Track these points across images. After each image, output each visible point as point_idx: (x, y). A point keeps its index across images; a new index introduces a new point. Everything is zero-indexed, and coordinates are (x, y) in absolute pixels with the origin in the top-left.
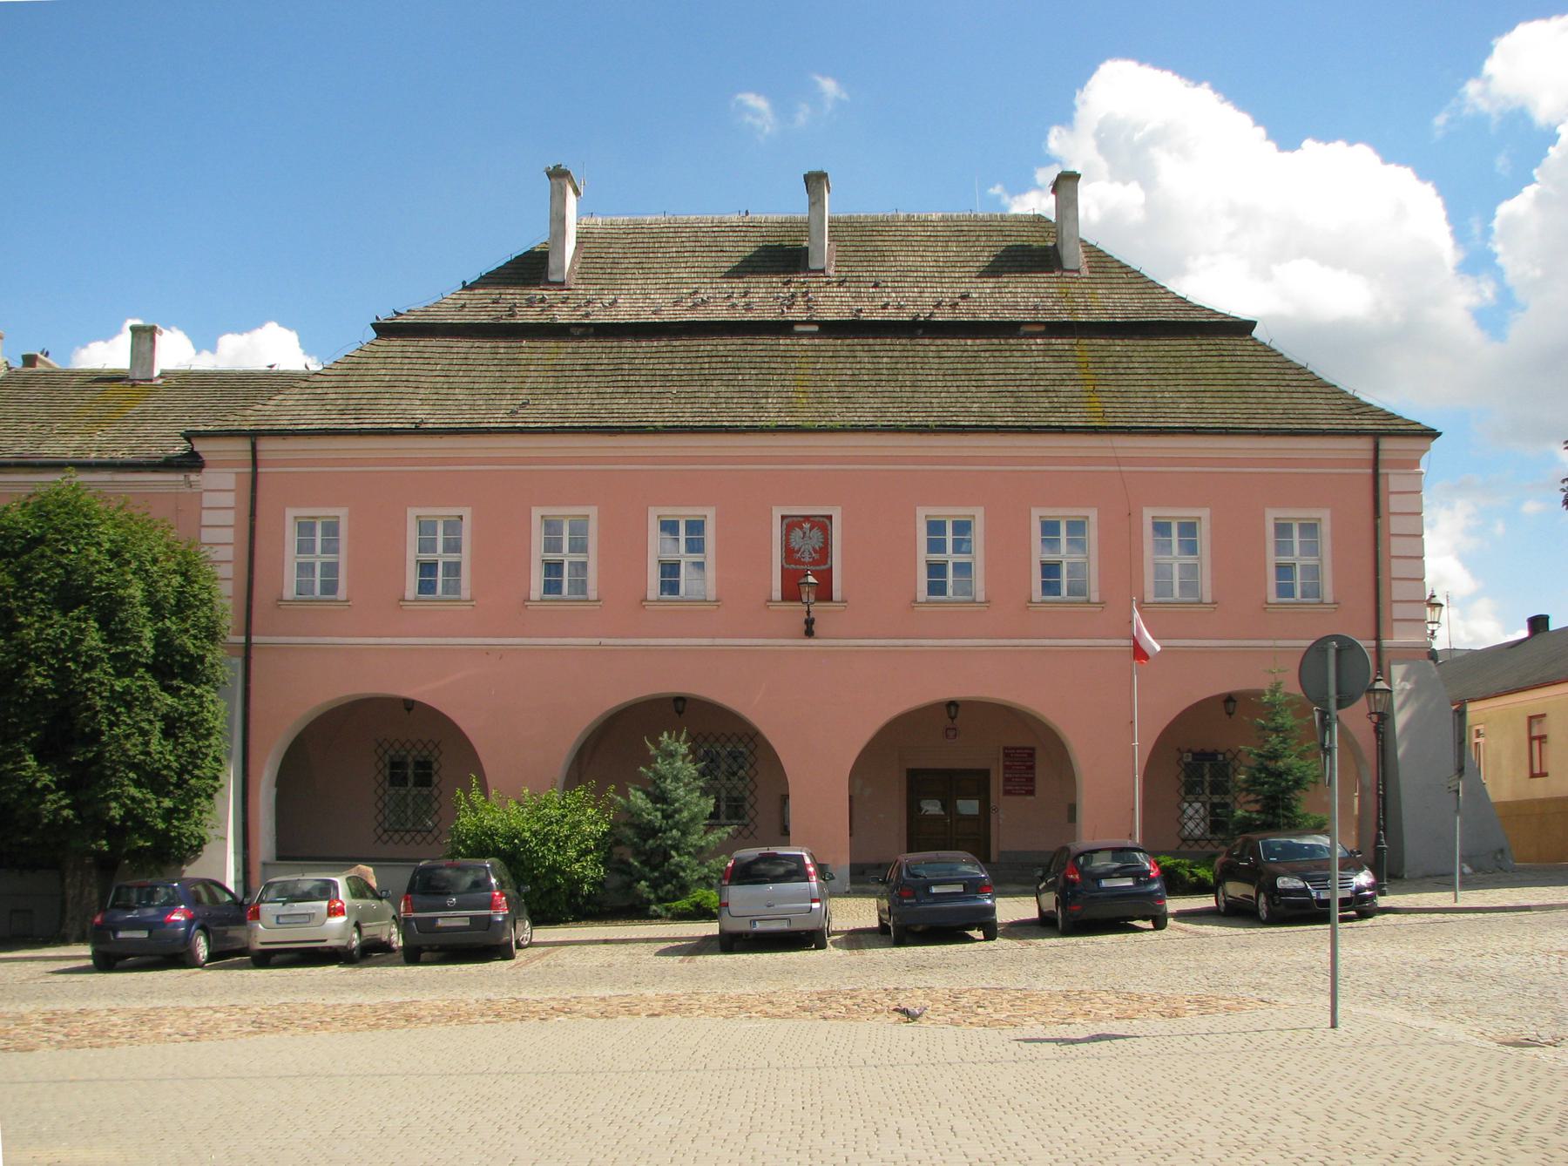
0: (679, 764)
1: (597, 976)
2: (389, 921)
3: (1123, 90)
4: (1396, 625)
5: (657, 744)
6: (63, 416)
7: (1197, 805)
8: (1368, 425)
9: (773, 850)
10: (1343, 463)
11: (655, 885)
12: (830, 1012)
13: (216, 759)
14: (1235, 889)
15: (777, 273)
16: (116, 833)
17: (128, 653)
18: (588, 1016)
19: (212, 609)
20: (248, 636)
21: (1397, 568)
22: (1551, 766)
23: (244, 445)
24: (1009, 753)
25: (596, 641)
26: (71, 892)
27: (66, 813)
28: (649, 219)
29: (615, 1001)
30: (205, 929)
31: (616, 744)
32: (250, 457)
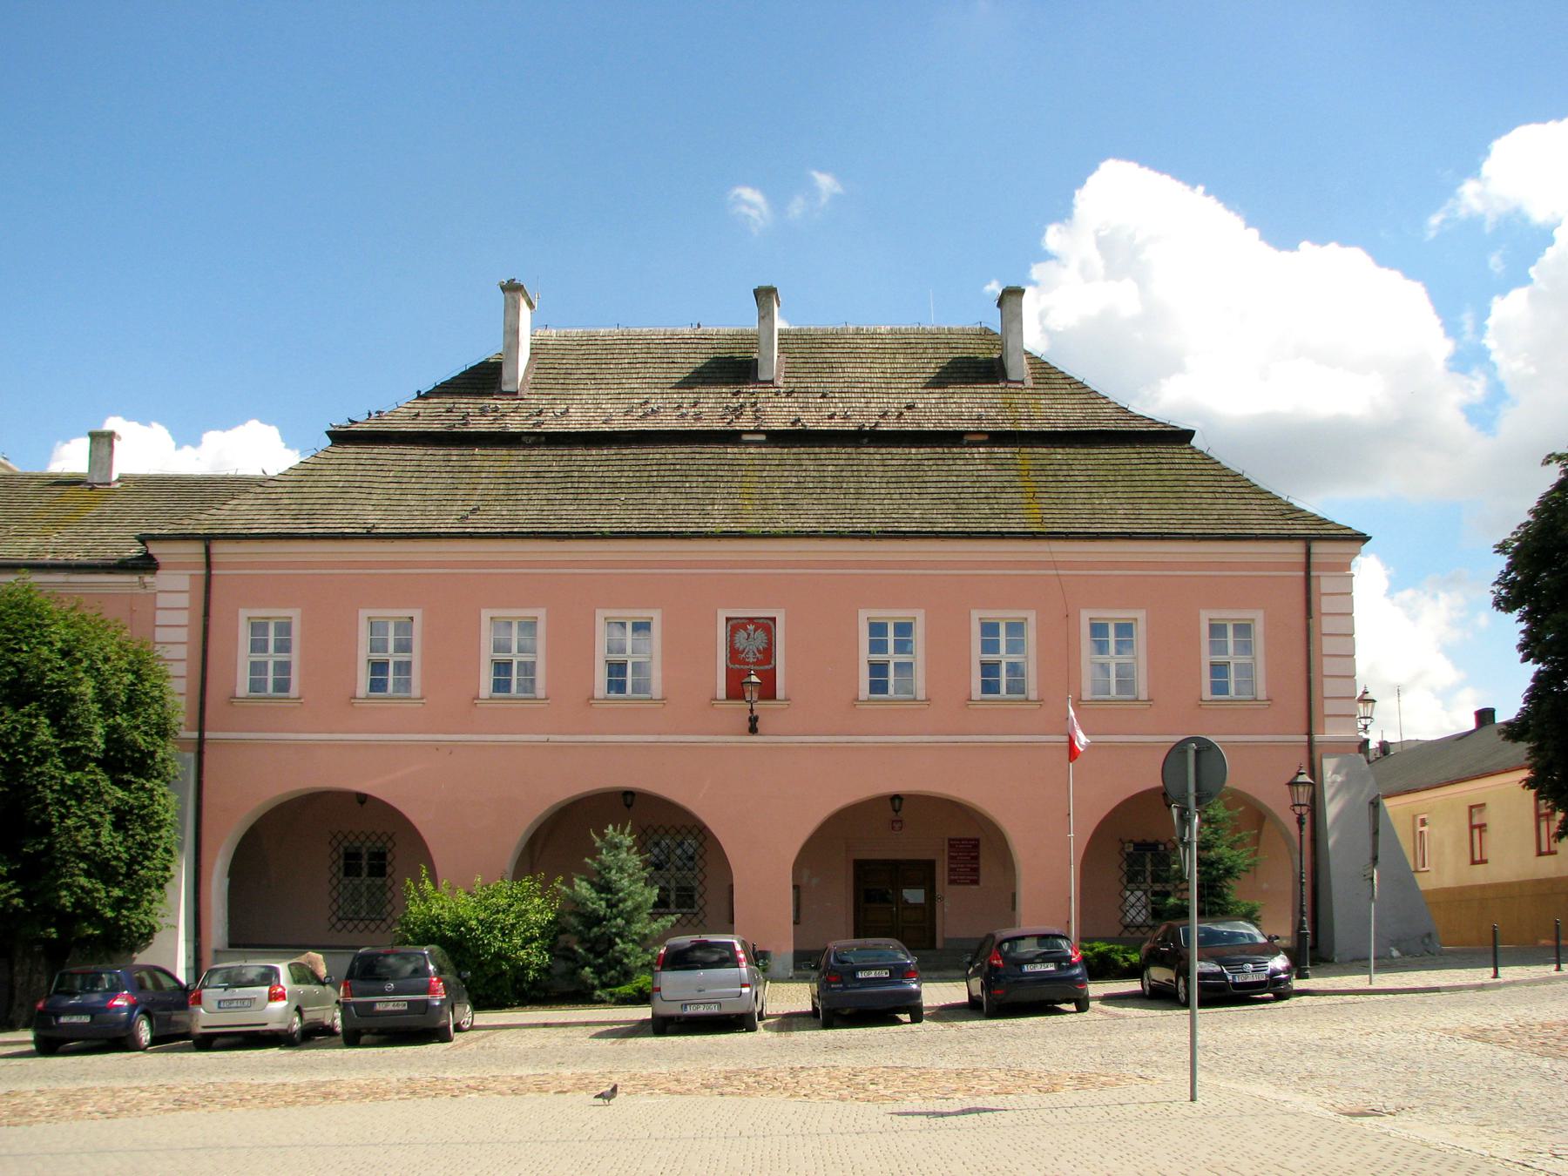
0: (624, 855)
1: (525, 1058)
2: (332, 1005)
3: (1119, 193)
4: (1327, 720)
5: (602, 836)
6: (19, 520)
7: (1139, 893)
8: (1300, 529)
9: (705, 937)
10: (1277, 566)
11: (599, 971)
12: (729, 1089)
13: (167, 851)
14: (1159, 974)
15: (727, 384)
16: (66, 921)
17: (77, 749)
18: (500, 1093)
19: (163, 706)
20: (201, 731)
21: (1329, 667)
22: (1490, 854)
23: (198, 548)
24: (954, 844)
25: (544, 738)
26: (19, 980)
27: (15, 901)
28: (602, 331)
29: (531, 1080)
30: (147, 1013)
31: (561, 837)
32: (203, 560)
